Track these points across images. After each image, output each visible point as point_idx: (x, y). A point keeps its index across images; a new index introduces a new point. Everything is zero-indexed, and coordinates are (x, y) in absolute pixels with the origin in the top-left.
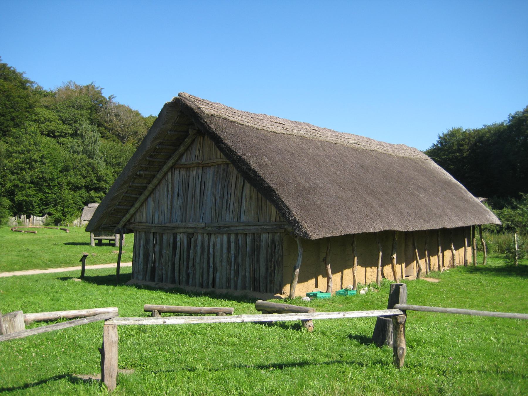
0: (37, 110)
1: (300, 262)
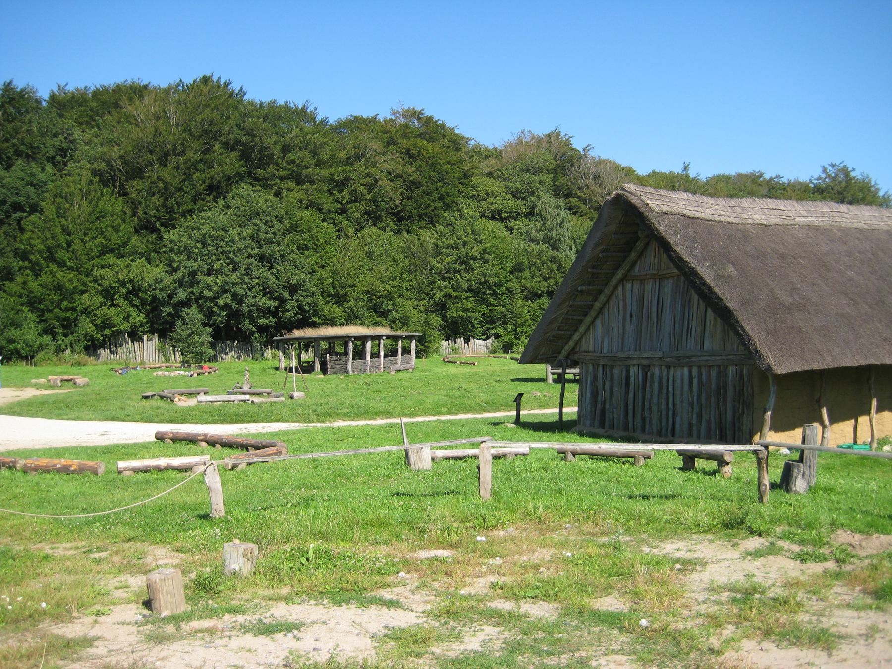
0: (475, 180)
1: (772, 402)
